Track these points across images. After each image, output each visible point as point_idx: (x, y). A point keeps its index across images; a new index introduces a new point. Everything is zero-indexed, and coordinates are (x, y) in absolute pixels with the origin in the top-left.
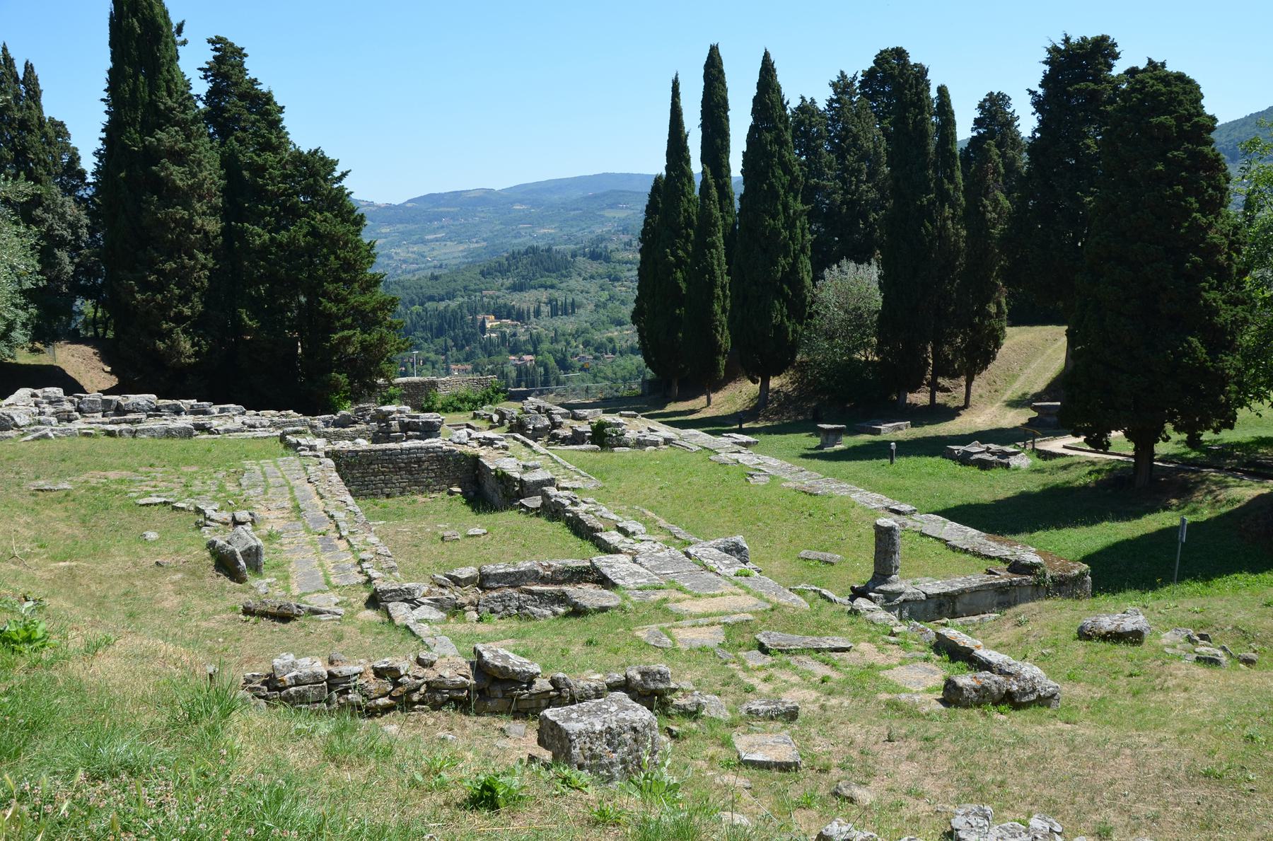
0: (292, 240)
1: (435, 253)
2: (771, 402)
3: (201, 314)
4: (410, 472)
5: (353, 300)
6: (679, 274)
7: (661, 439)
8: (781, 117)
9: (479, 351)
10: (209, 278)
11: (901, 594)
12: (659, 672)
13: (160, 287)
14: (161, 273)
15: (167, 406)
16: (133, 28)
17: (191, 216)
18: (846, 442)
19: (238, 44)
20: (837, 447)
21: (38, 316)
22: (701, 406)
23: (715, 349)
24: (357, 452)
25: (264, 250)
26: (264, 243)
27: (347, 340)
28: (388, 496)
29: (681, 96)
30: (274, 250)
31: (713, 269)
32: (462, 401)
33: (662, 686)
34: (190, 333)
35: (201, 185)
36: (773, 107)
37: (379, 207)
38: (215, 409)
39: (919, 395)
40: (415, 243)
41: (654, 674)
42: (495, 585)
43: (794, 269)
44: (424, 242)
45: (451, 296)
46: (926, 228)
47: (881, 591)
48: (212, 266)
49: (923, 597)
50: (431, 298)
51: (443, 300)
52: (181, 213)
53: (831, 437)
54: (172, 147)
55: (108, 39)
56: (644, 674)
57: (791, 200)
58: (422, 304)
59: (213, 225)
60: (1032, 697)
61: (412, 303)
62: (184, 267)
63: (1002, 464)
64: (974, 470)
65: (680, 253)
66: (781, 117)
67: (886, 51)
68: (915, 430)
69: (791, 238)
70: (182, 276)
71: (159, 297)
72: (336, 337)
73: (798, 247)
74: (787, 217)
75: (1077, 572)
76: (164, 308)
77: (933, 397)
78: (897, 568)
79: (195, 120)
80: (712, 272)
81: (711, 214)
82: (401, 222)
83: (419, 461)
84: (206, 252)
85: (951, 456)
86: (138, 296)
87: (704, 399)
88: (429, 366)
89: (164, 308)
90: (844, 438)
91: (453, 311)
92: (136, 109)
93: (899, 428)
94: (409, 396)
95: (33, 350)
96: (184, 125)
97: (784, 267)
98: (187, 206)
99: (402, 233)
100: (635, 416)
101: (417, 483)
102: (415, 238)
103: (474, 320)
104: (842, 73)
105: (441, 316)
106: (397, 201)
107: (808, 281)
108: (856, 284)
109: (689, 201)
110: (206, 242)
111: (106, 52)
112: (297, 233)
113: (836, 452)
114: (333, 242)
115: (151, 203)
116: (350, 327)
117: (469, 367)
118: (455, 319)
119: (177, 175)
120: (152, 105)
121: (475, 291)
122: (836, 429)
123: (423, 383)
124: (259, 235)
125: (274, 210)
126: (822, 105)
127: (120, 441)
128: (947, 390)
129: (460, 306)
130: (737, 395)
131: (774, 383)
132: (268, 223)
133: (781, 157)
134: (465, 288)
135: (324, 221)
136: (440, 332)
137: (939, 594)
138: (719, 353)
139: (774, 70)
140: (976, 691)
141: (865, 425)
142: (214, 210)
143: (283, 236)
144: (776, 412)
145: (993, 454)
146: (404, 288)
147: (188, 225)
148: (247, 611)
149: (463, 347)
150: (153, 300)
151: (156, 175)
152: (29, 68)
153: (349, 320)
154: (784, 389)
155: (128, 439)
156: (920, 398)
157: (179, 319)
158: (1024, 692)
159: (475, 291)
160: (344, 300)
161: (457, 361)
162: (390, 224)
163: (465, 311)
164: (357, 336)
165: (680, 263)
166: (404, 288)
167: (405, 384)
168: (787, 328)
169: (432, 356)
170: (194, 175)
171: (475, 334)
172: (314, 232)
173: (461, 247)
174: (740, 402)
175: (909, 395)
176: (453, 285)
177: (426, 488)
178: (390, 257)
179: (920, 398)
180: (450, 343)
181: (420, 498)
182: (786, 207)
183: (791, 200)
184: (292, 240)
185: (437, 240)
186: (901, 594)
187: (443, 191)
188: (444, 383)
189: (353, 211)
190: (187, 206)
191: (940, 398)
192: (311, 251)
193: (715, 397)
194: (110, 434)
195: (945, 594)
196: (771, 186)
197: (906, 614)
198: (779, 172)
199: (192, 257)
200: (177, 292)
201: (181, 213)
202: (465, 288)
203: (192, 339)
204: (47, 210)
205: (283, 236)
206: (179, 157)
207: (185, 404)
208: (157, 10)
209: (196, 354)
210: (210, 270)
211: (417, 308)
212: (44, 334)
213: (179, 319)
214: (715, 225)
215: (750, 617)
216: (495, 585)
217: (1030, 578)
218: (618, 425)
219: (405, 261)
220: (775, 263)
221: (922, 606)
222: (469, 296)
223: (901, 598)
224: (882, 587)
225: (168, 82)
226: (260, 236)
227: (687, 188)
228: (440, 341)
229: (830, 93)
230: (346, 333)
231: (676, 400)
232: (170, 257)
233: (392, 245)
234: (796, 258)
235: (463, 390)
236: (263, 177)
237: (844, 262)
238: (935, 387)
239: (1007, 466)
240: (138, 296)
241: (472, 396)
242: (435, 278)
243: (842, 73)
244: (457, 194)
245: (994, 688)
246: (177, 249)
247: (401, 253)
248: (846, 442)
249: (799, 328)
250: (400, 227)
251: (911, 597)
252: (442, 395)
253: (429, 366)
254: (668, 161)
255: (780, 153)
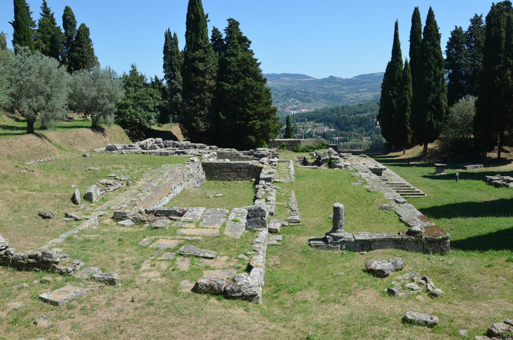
0: (238, 88)
1: (362, 96)
2: (428, 154)
3: (208, 114)
4: (237, 172)
5: (258, 109)
6: (394, 101)
7: (343, 165)
8: (435, 35)
9: (374, 132)
10: (211, 101)
11: (342, 238)
12: (49, 254)
13: (194, 105)
14: (194, 100)
15: (192, 146)
16: (192, 17)
17: (205, 80)
18: (447, 172)
19: (237, 20)
20: (442, 174)
21: (160, 115)
22: (402, 155)
23: (406, 132)
24: (218, 163)
25: (228, 92)
26: (229, 89)
27: (254, 124)
28: (229, 180)
29: (399, 29)
30: (232, 91)
31: (406, 99)
32: (309, 148)
33: (50, 260)
34: (203, 120)
35: (208, 68)
36: (432, 30)
37: (343, 79)
38: (208, 147)
39: (494, 154)
40: (356, 93)
41: (47, 254)
42: (160, 215)
43: (438, 98)
44: (358, 92)
45: (365, 112)
46: (497, 80)
47: (332, 236)
48: (215, 98)
49: (353, 240)
50: (358, 113)
51: (362, 113)
52: (201, 79)
53: (440, 169)
54: (200, 57)
55: (185, 21)
56: (43, 253)
57: (437, 69)
58: (355, 115)
59: (212, 83)
60: (238, 294)
61: (351, 114)
62: (202, 98)
63: (506, 185)
64: (492, 187)
65: (395, 92)
66: (435, 35)
67: (500, 3)
68: (484, 168)
69: (436, 85)
70: (201, 101)
71: (193, 108)
72: (250, 123)
73: (440, 89)
74: (435, 76)
75: (441, 237)
76: (195, 113)
77: (499, 155)
78: (341, 226)
79: (208, 47)
80: (406, 100)
81: (407, 76)
82: (351, 85)
83: (240, 168)
84: (210, 92)
85: (485, 180)
86: (187, 108)
87: (402, 152)
88: (355, 137)
89: (195, 113)
90: (446, 170)
91: (366, 117)
92: (191, 45)
93: (477, 167)
94: (290, 146)
95: (158, 126)
96: (204, 49)
97: (433, 98)
98: (204, 77)
99: (351, 89)
100: (366, 157)
101: (240, 176)
102: (355, 91)
103: (373, 121)
104: (476, 14)
105: (361, 119)
106: (350, 77)
107: (445, 103)
108: (468, 104)
109: (400, 71)
110: (210, 89)
111: (185, 26)
112: (240, 86)
113: (440, 176)
114: (252, 88)
115: (192, 76)
116: (256, 119)
117: (370, 138)
118: (366, 120)
119: (201, 66)
120: (197, 42)
121: (374, 110)
122: (442, 166)
123: (295, 141)
124: (228, 86)
125: (233, 77)
126: (465, 29)
127: (146, 155)
128: (508, 152)
129: (368, 116)
130: (416, 151)
131: (430, 146)
132: (231, 82)
133: (434, 51)
134: (371, 109)
135: (249, 80)
136: (360, 125)
137: (361, 240)
138: (408, 133)
139: (434, 15)
140: (206, 286)
141: (461, 165)
142: (214, 78)
143: (235, 87)
144: (429, 158)
145: (504, 181)
146: (349, 109)
147: (204, 83)
148: (40, 215)
149: (368, 131)
150: (192, 109)
151: (194, 66)
152: (175, 35)
153: (256, 117)
154: (435, 149)
155: (148, 155)
156: (493, 155)
157: (200, 116)
158: (233, 291)
159: (374, 110)
160: (255, 110)
161: (366, 136)
162: (347, 86)
163: (370, 117)
164: (259, 123)
165: (394, 96)
166: (349, 109)
167: (289, 141)
168: (433, 123)
169: (357, 134)
170: (206, 66)
171: (373, 126)
172: (246, 85)
173: (372, 94)
174: (416, 153)
175: (488, 154)
176: (367, 108)
177: (243, 178)
178: (346, 98)
179: (493, 155)
180: (364, 129)
181: (240, 182)
182: (435, 72)
183: (437, 69)
184: (238, 88)
185: (363, 91)
186: (342, 238)
187: (367, 73)
188: (303, 141)
189: (261, 77)
190: (204, 77)
191: (503, 155)
192: (244, 92)
193: (407, 151)
194: (143, 153)
195: (365, 241)
196: (429, 64)
197: (344, 247)
198: (433, 58)
199: (204, 94)
200: (199, 106)
201: (201, 79)
202: (371, 109)
203: (204, 123)
204: (176, 80)
205: (235, 87)
206: (202, 60)
207: (198, 145)
208: (200, 11)
209: (206, 128)
210: (212, 99)
211: (353, 116)
212: (162, 120)
213: (200, 116)
214: (408, 81)
215: (199, 238)
216: (160, 215)
217: (413, 238)
218: (337, 159)
219: (351, 99)
220: (429, 96)
221: (353, 245)
222: (372, 112)
223: (342, 240)
224: (333, 234)
225: (201, 35)
226: (228, 86)
227: (399, 66)
228: (360, 128)
229: (469, 24)
230: (255, 121)
231: (393, 152)
232: (199, 94)
233: (347, 93)
234: (439, 94)
235: (310, 144)
236: (230, 66)
237: (468, 96)
238: (501, 150)
239: (508, 186)
240: (187, 108)
241: (314, 147)
242: (360, 105)
243: (476, 14)
244: (372, 74)
245: (216, 287)
246: (201, 91)
247: (350, 96)
248: (447, 172)
249: (440, 123)
250: (351, 87)
251: (346, 240)
252: (302, 146)
253: (355, 137)
254: (392, 55)
255: (433, 49)
